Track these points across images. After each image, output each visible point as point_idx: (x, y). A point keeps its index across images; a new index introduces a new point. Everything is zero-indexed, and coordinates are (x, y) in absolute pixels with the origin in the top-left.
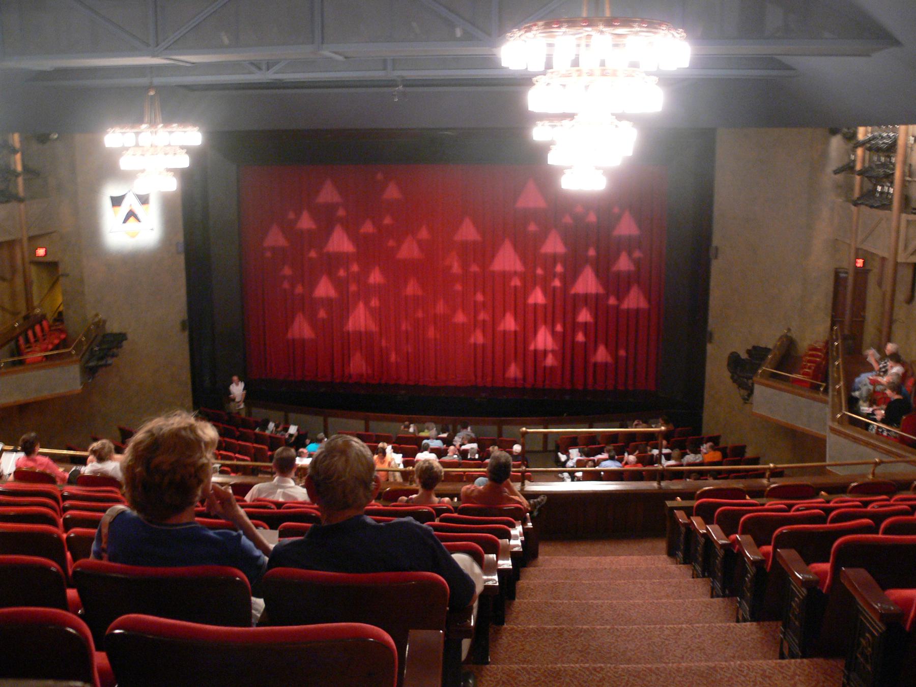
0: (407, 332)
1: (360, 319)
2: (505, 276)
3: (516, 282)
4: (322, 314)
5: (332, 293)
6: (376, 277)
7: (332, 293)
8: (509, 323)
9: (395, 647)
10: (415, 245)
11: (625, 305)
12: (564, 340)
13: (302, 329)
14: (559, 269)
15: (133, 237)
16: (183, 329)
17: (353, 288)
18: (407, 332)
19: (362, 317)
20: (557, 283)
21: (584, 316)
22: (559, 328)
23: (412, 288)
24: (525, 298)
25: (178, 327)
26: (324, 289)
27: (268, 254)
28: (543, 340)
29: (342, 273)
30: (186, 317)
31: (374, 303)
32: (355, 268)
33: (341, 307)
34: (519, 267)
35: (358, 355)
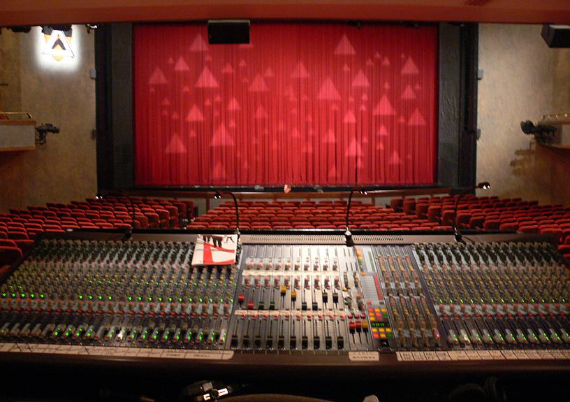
0: (335, 112)
1: (221, 137)
2: (327, 103)
3: (334, 107)
4: (193, 134)
5: (201, 118)
6: (233, 105)
7: (201, 118)
8: (331, 138)
9: (21, 251)
10: (263, 83)
11: (411, 123)
12: (369, 149)
13: (178, 146)
14: (365, 97)
15: (58, 60)
16: (93, 138)
17: (216, 113)
18: (335, 112)
19: (224, 135)
20: (363, 108)
21: (383, 131)
22: (365, 140)
23: (260, 113)
24: (342, 118)
25: (89, 135)
26: (195, 115)
27: (152, 90)
28: (354, 149)
29: (208, 103)
30: (95, 129)
31: (232, 124)
32: (218, 99)
33: (206, 129)
34: (338, 97)
35: (219, 164)
